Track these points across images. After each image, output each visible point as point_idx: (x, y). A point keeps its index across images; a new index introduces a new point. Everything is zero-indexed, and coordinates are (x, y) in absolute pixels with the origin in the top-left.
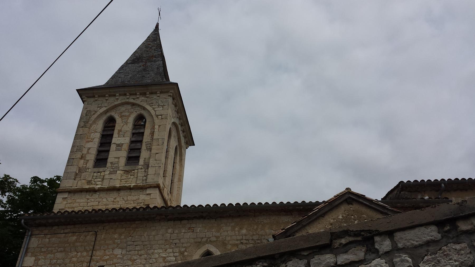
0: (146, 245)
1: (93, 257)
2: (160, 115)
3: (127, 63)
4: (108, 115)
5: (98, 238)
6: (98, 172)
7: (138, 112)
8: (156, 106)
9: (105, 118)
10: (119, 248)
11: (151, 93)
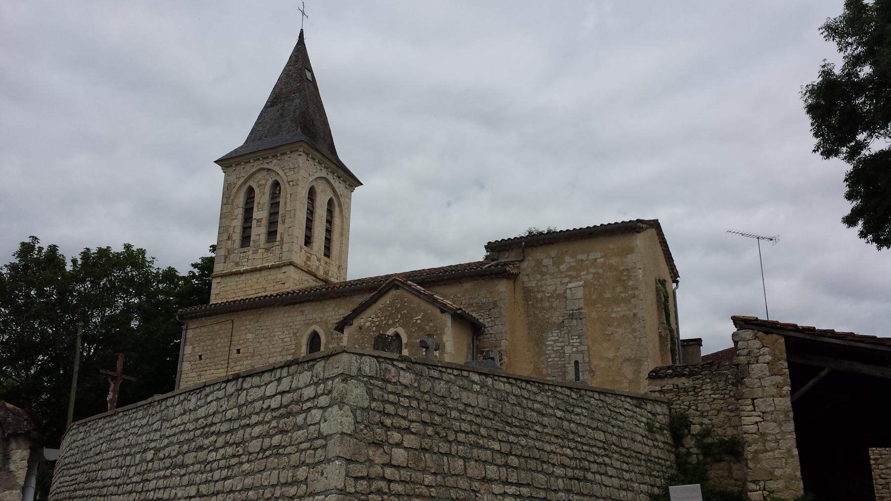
0: (269, 329)
1: (232, 343)
2: (291, 181)
3: (266, 107)
4: (247, 185)
5: (235, 326)
6: (244, 252)
7: (273, 179)
8: (288, 170)
9: (245, 189)
10: (250, 333)
11: (283, 154)
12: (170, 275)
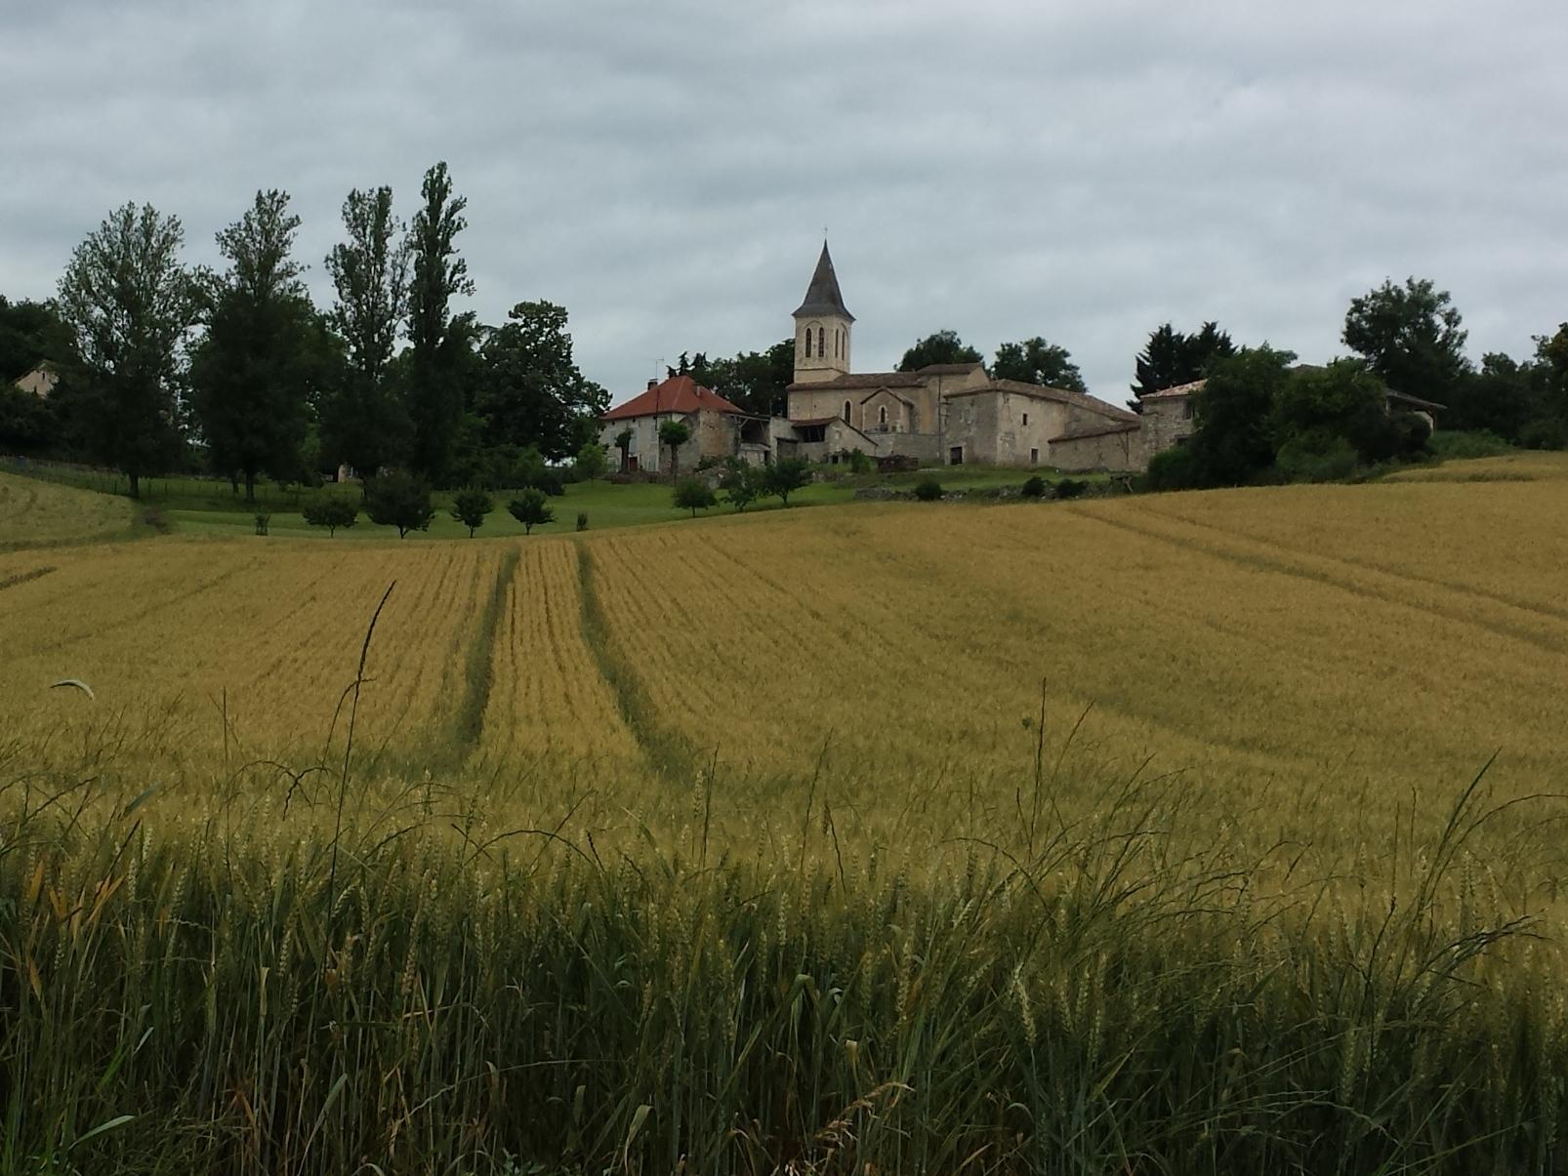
12: (1180, 337)
